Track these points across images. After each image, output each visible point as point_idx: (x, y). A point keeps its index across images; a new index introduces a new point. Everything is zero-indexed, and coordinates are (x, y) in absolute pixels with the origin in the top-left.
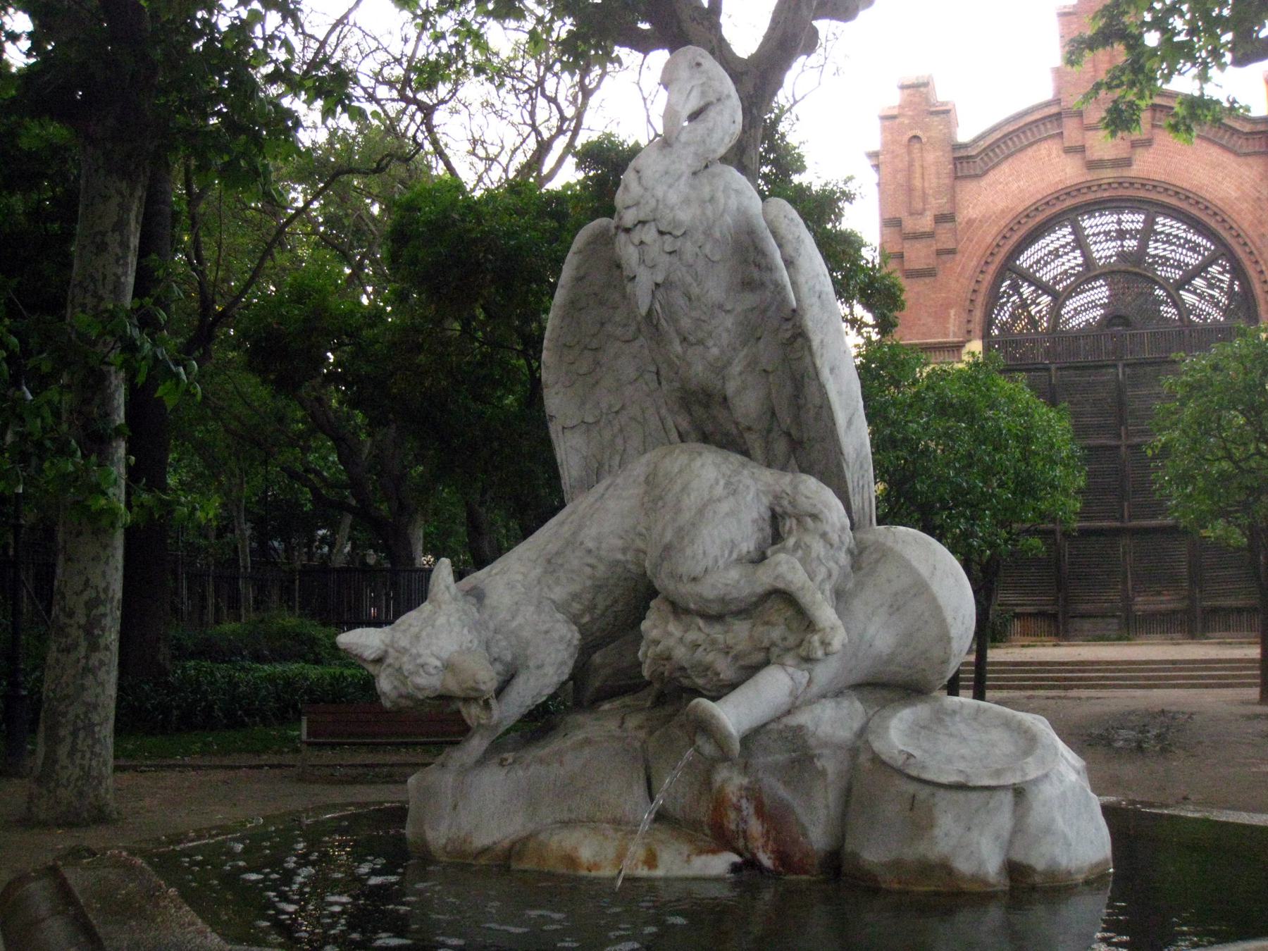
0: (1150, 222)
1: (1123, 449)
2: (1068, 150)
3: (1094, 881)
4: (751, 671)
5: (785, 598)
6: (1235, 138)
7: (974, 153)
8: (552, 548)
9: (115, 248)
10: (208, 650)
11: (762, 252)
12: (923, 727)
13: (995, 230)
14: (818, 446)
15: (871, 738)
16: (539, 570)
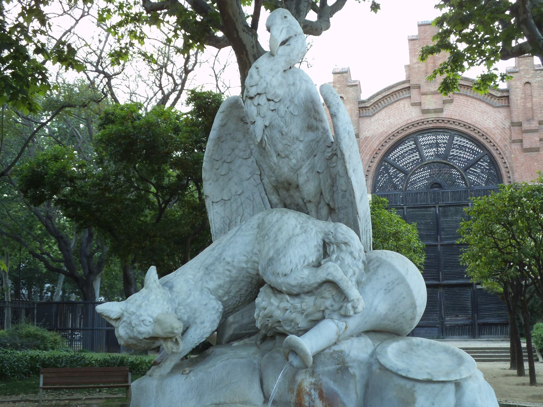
0: (451, 139)
1: (439, 247)
2: (413, 104)
4: (315, 322)
6: (493, 99)
8: (209, 261)
11: (317, 112)
12: (404, 352)
13: (377, 143)
14: (342, 211)
15: (378, 357)
16: (201, 273)
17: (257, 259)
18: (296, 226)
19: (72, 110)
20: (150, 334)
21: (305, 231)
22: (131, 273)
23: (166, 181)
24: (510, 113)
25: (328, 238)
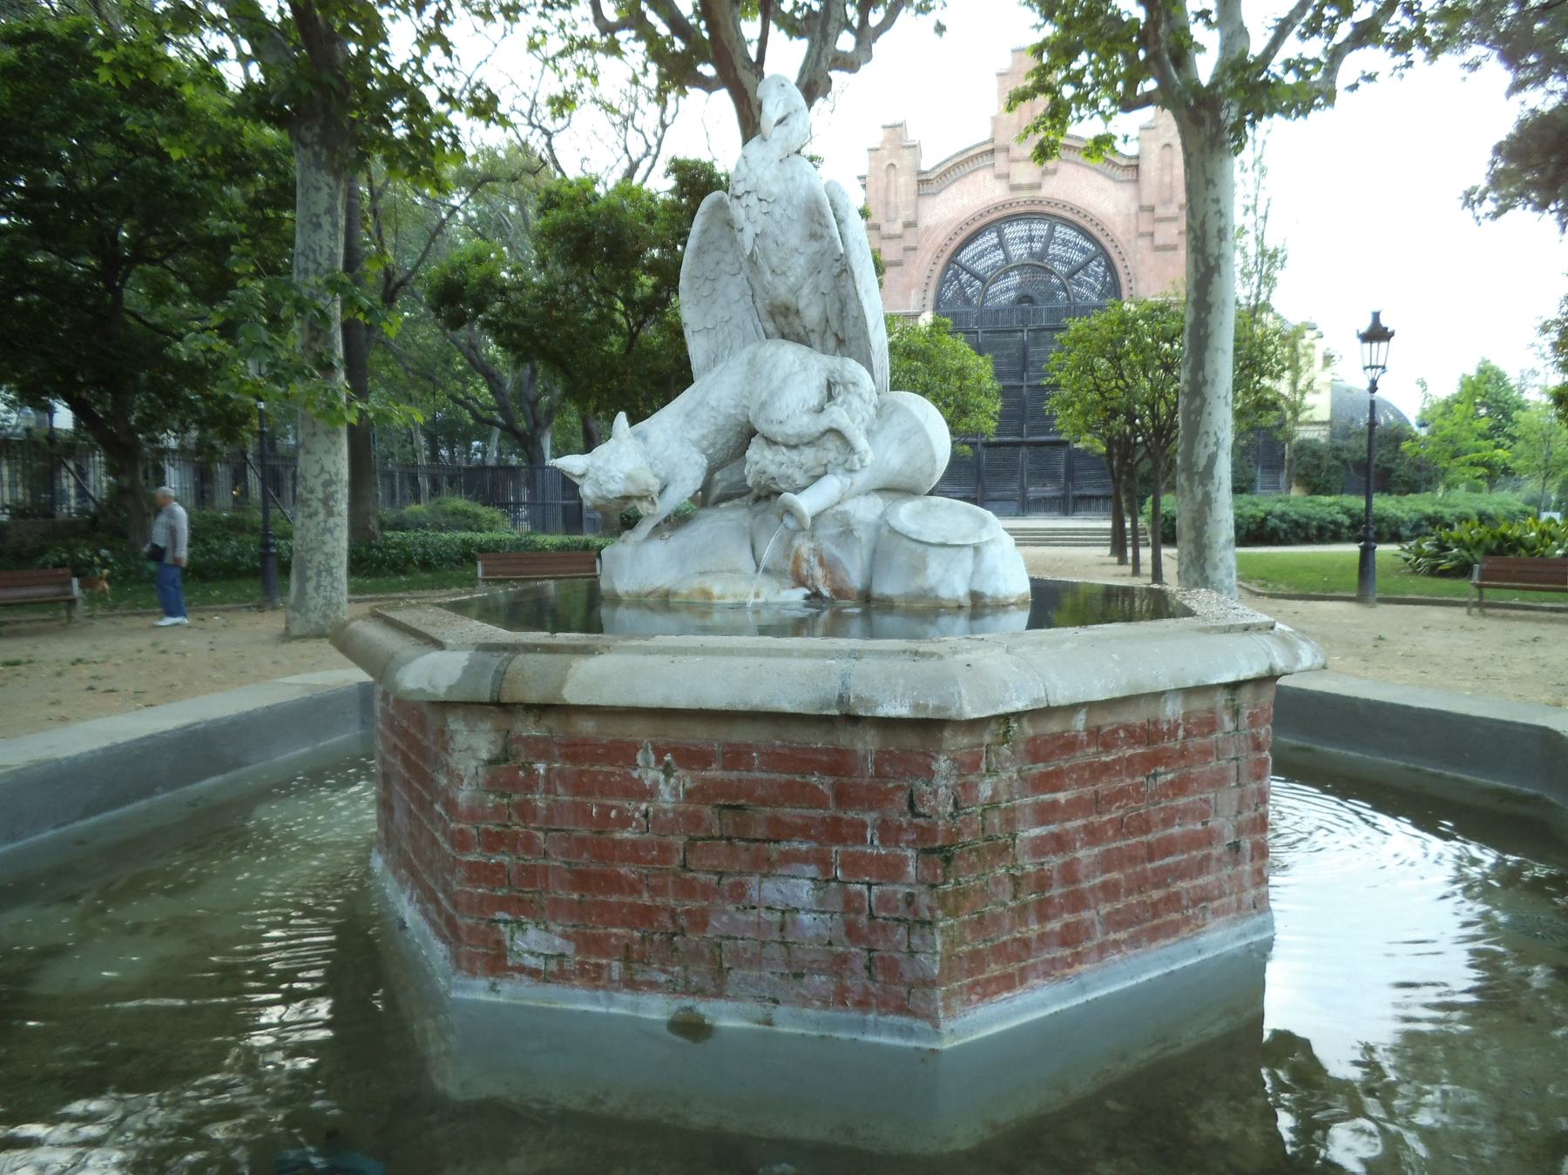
0: (1052, 230)
2: (998, 177)
3: (1019, 604)
4: (817, 478)
5: (836, 433)
9: (327, 226)
10: (399, 525)
11: (822, 215)
19: (496, 185)
21: (805, 369)
22: (593, 425)
23: (638, 294)
24: (1139, 192)
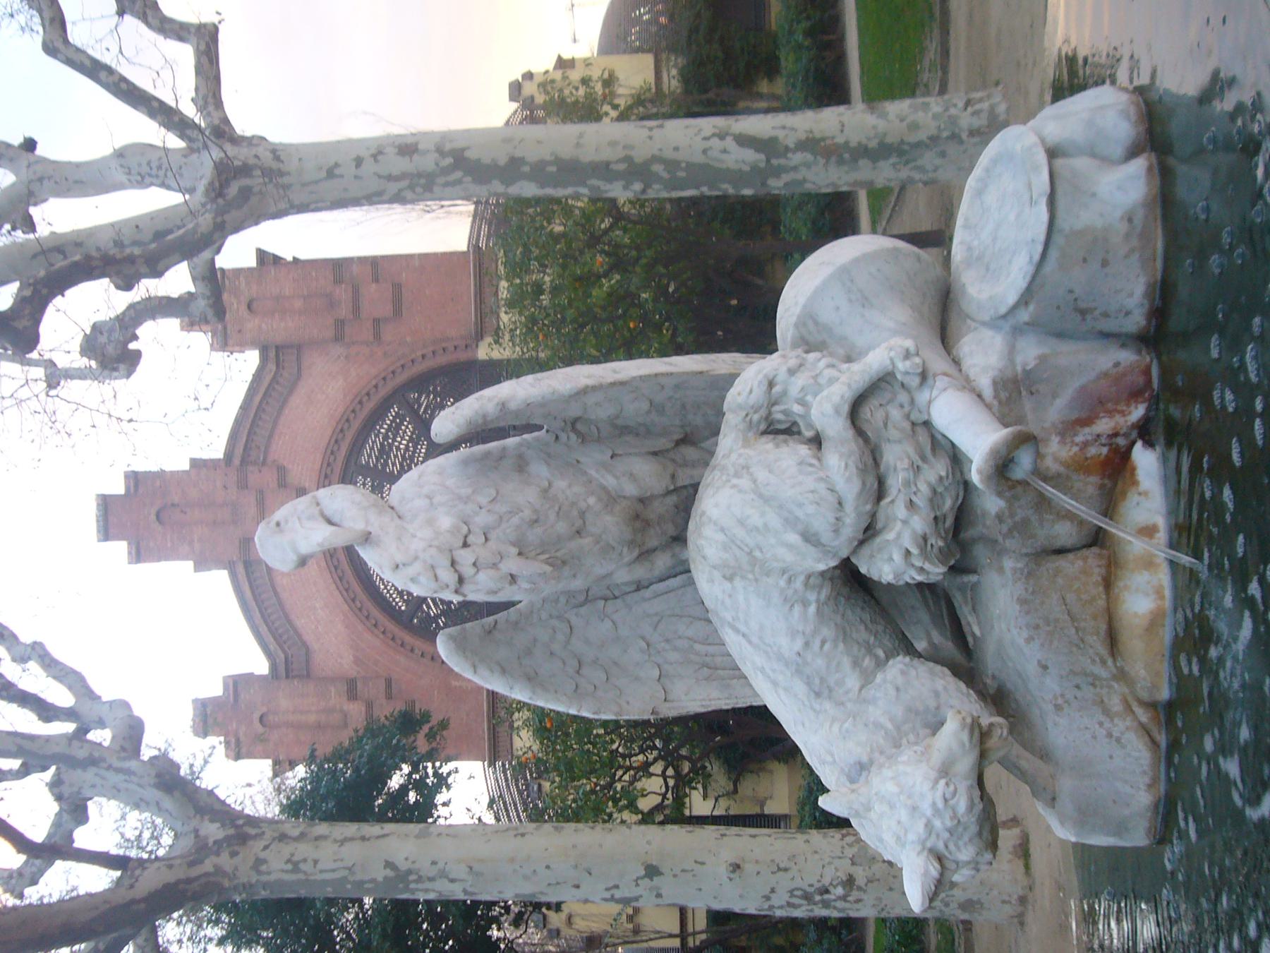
6: (281, 380)
7: (282, 656)
13: (368, 636)
14: (690, 417)
17: (802, 578)
18: (734, 486)
20: (972, 786)
25: (759, 422)
